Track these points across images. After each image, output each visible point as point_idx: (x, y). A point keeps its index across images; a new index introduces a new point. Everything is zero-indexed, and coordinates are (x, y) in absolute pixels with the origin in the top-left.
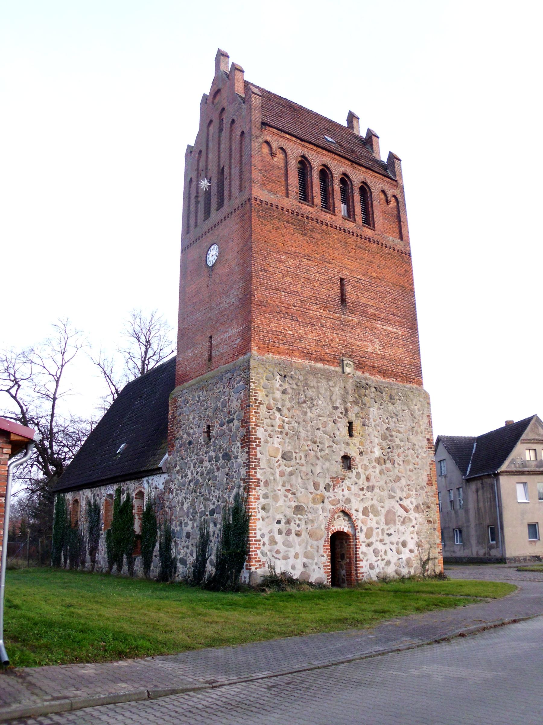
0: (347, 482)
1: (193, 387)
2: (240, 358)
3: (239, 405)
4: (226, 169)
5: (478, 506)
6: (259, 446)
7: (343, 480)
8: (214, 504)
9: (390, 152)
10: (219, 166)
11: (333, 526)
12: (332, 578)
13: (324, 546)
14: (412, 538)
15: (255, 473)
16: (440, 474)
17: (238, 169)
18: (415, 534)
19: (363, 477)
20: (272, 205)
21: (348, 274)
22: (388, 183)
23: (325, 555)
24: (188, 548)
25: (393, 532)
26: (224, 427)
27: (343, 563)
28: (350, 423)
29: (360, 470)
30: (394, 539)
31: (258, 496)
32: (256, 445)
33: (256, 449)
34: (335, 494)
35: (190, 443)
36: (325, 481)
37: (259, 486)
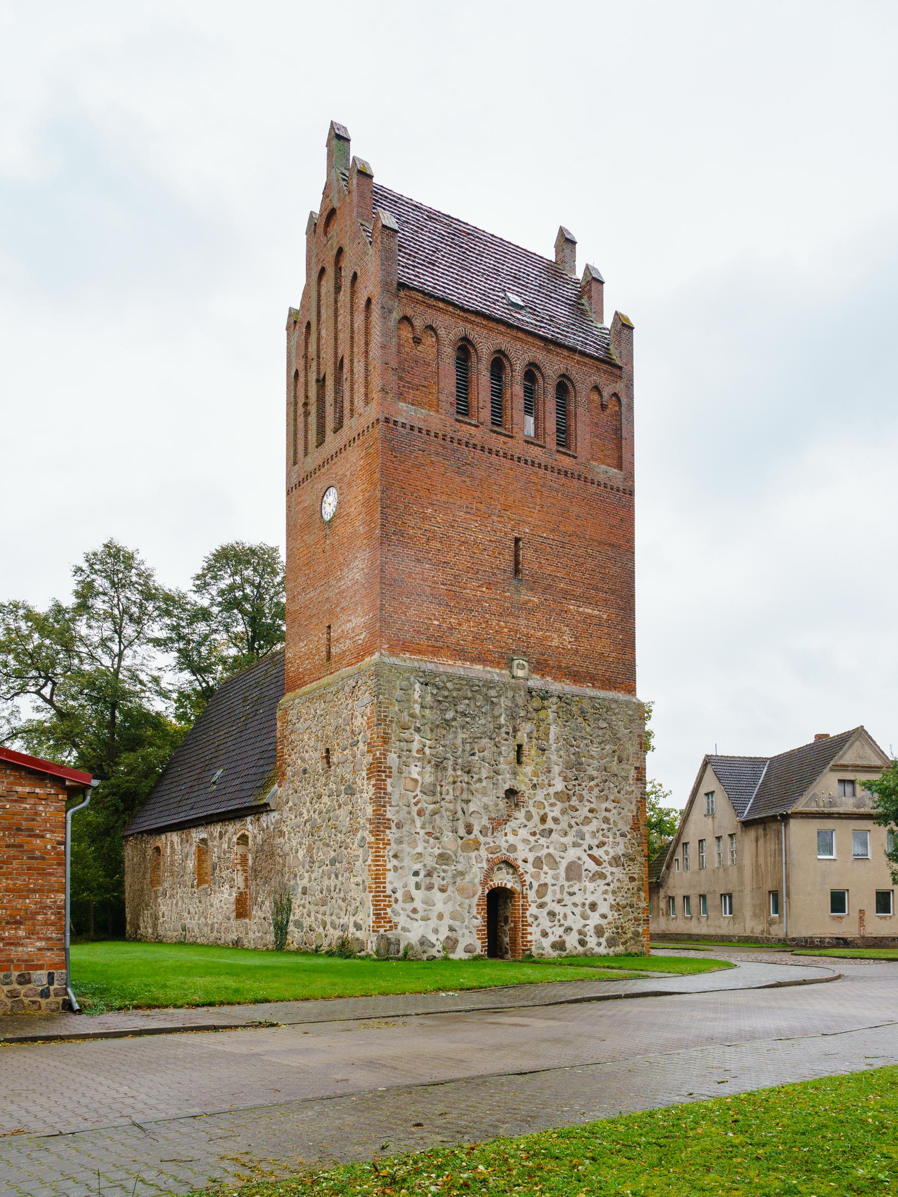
0: (513, 824)
1: (308, 696)
2: (367, 659)
3: (365, 724)
4: (346, 361)
5: (757, 861)
6: (390, 777)
7: (506, 821)
8: (335, 851)
9: (616, 313)
10: (336, 356)
11: (491, 880)
12: (488, 946)
13: (478, 905)
14: (605, 900)
15: (385, 811)
16: (706, 813)
17: (362, 364)
18: (610, 894)
19: (536, 818)
20: (412, 428)
21: (527, 531)
22: (605, 372)
23: (479, 916)
24: (304, 907)
25: (576, 891)
26: (347, 751)
27: (506, 928)
28: (520, 746)
29: (531, 809)
30: (578, 899)
31: (389, 840)
32: (386, 776)
33: (385, 780)
34: (495, 839)
35: (305, 771)
36: (480, 822)
37: (390, 828)
